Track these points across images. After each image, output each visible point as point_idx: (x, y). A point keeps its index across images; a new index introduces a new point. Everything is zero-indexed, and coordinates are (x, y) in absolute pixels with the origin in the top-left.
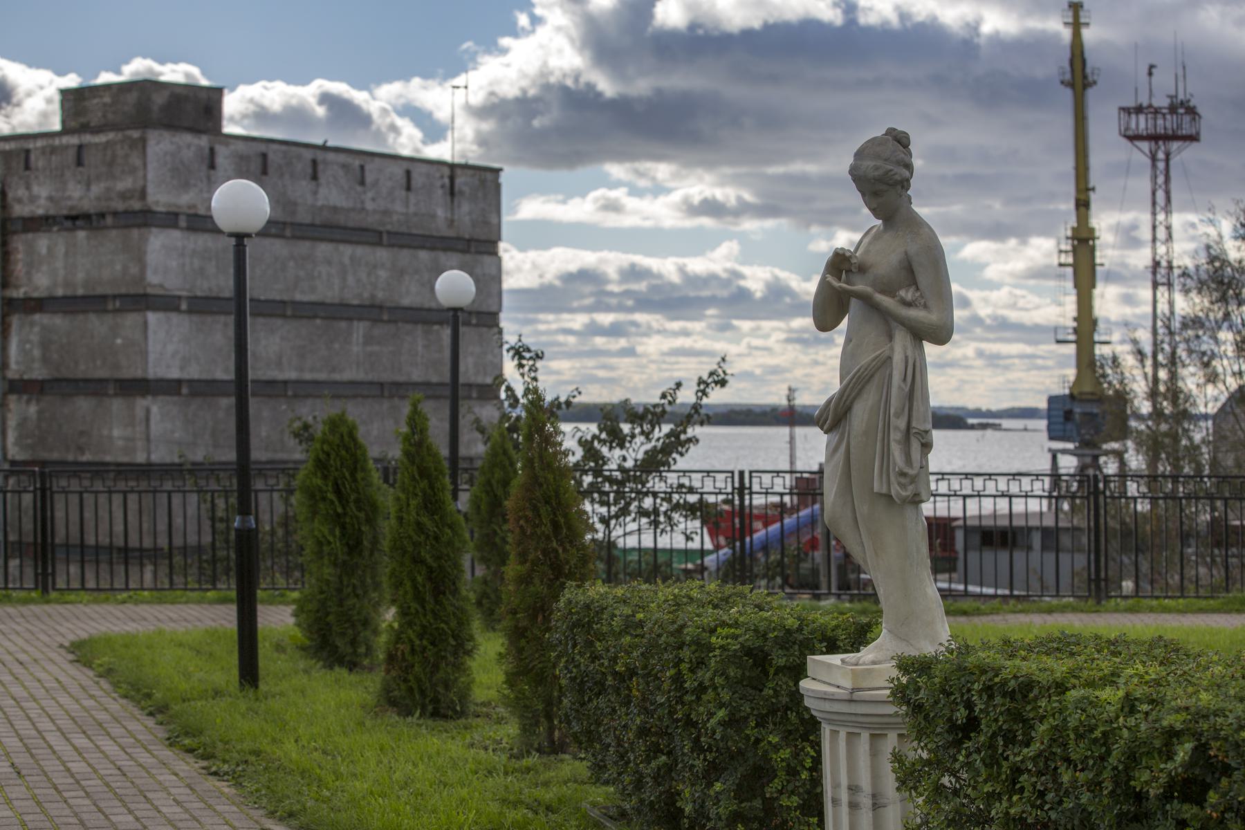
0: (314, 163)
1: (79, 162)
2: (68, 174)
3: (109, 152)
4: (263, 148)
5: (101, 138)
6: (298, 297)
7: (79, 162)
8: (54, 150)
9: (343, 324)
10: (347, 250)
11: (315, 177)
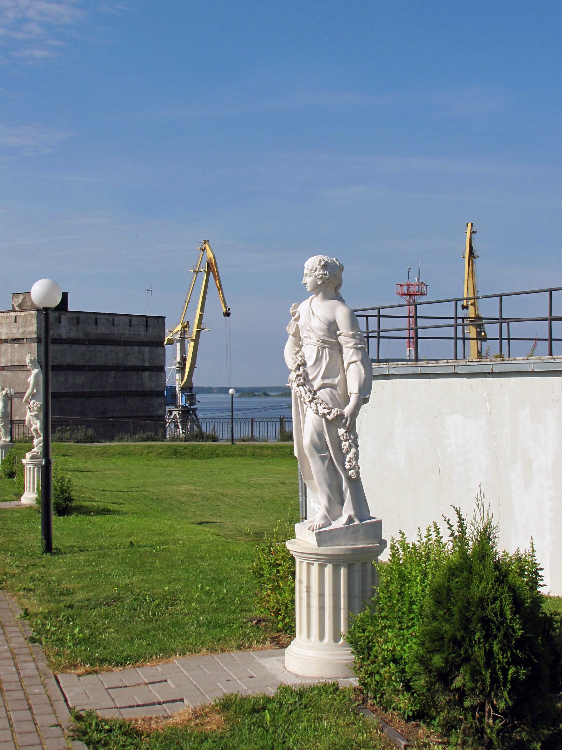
0: (96, 319)
1: (16, 322)
2: (12, 325)
3: (25, 318)
4: (78, 315)
5: (23, 313)
6: (90, 364)
7: (16, 322)
8: (7, 317)
9: (106, 372)
10: (108, 348)
11: (96, 324)
